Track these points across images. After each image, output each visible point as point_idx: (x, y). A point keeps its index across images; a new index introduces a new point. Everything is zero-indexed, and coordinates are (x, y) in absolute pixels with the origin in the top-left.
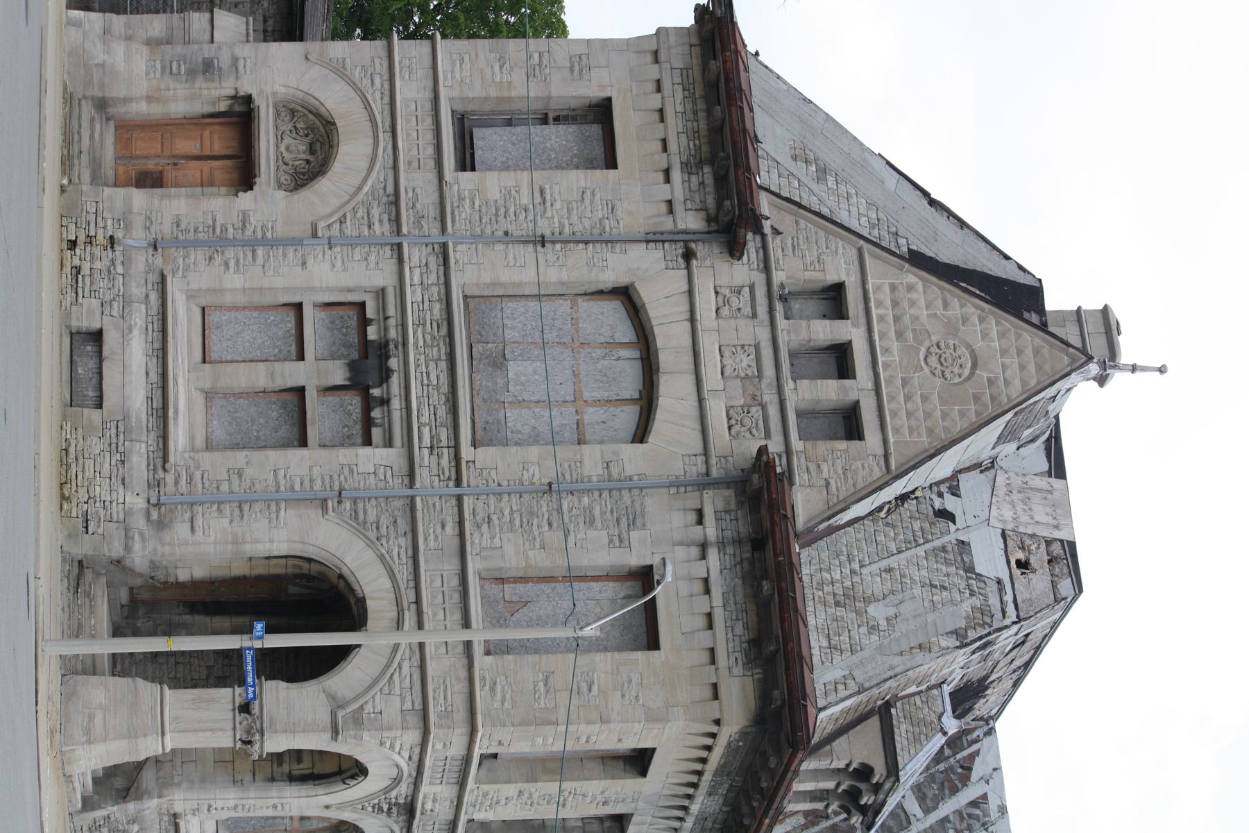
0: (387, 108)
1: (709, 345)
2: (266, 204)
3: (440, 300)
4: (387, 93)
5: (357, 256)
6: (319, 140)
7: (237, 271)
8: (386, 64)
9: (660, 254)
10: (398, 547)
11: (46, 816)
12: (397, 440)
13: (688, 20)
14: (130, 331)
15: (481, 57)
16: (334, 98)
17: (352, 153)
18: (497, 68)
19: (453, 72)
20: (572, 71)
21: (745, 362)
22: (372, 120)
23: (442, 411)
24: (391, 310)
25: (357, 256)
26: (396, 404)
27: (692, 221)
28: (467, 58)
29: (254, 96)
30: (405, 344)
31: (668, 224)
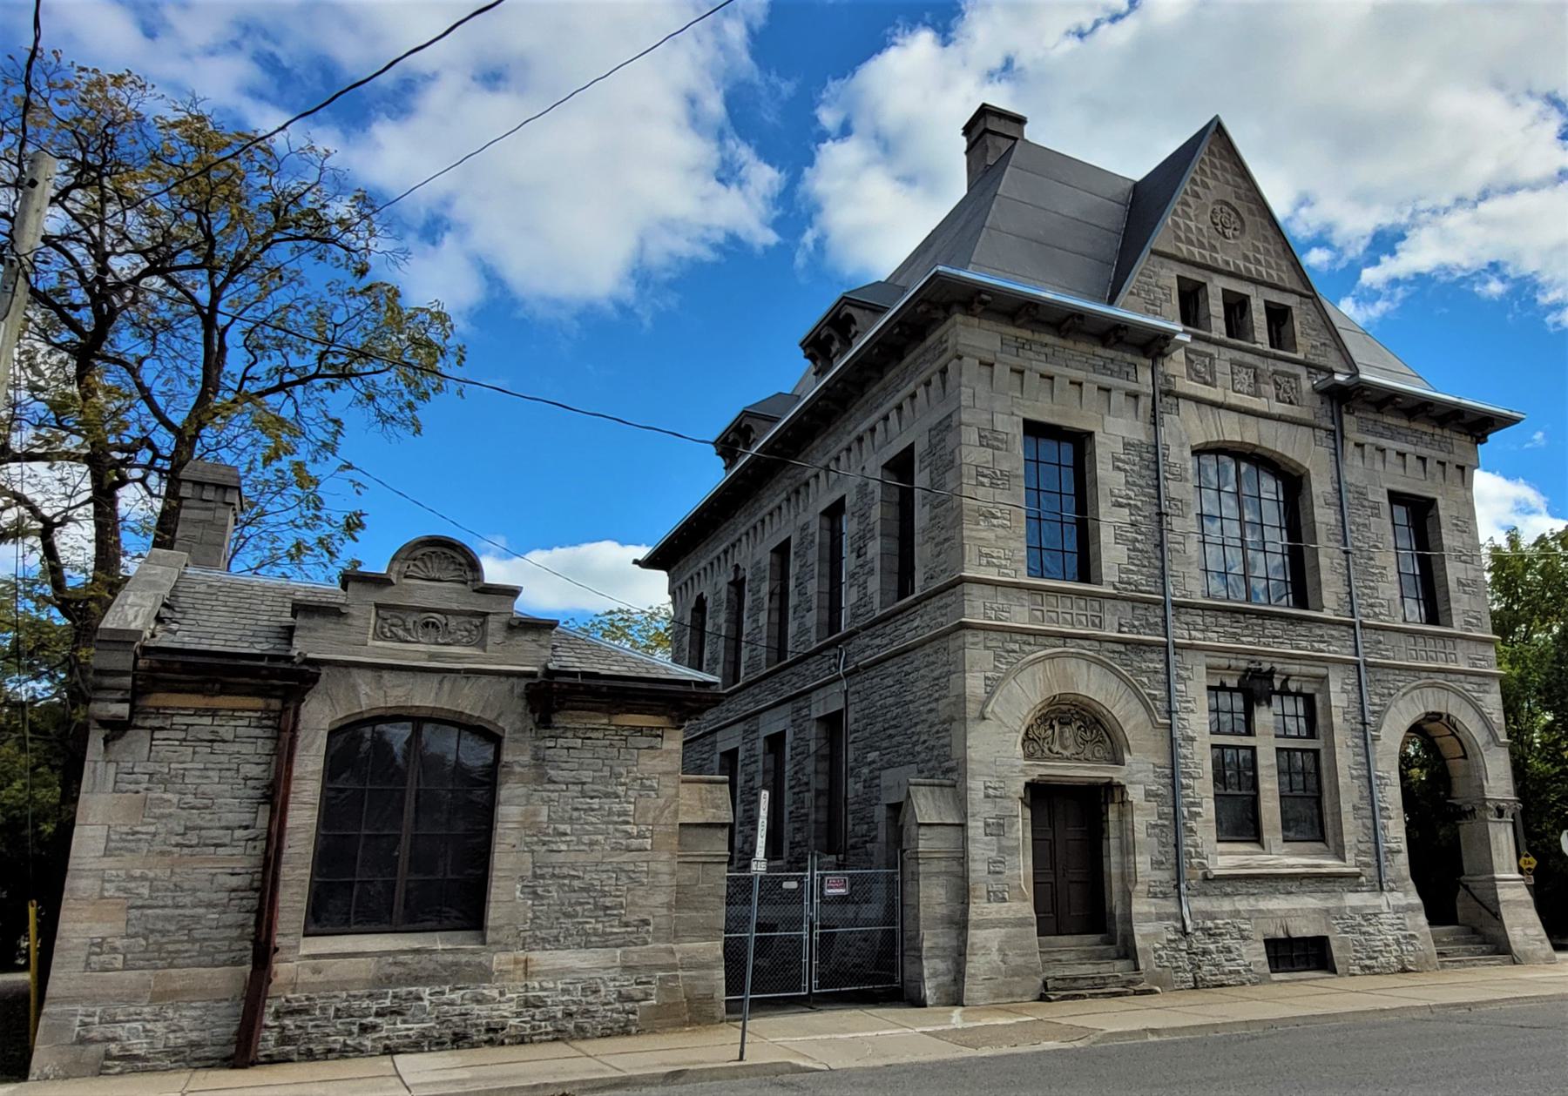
0: (1040, 640)
1: (1234, 399)
2: (1138, 774)
3: (1216, 617)
4: (1025, 638)
5: (1181, 687)
6: (1070, 716)
7: (1199, 805)
8: (993, 635)
9: (1166, 417)
10: (1403, 682)
11: (474, 1062)
12: (1322, 671)
13: (808, 362)
14: (1260, 911)
15: (984, 534)
16: (1025, 695)
17: (1093, 684)
18: (995, 521)
19: (999, 567)
20: (998, 449)
21: (1243, 375)
22: (1051, 657)
23: (1301, 630)
24: (1224, 662)
25: (1181, 687)
26: (1294, 668)
27: (1144, 380)
28: (984, 550)
29: (1028, 779)
30: (1255, 653)
31: (1145, 403)
